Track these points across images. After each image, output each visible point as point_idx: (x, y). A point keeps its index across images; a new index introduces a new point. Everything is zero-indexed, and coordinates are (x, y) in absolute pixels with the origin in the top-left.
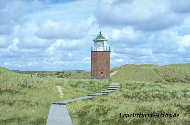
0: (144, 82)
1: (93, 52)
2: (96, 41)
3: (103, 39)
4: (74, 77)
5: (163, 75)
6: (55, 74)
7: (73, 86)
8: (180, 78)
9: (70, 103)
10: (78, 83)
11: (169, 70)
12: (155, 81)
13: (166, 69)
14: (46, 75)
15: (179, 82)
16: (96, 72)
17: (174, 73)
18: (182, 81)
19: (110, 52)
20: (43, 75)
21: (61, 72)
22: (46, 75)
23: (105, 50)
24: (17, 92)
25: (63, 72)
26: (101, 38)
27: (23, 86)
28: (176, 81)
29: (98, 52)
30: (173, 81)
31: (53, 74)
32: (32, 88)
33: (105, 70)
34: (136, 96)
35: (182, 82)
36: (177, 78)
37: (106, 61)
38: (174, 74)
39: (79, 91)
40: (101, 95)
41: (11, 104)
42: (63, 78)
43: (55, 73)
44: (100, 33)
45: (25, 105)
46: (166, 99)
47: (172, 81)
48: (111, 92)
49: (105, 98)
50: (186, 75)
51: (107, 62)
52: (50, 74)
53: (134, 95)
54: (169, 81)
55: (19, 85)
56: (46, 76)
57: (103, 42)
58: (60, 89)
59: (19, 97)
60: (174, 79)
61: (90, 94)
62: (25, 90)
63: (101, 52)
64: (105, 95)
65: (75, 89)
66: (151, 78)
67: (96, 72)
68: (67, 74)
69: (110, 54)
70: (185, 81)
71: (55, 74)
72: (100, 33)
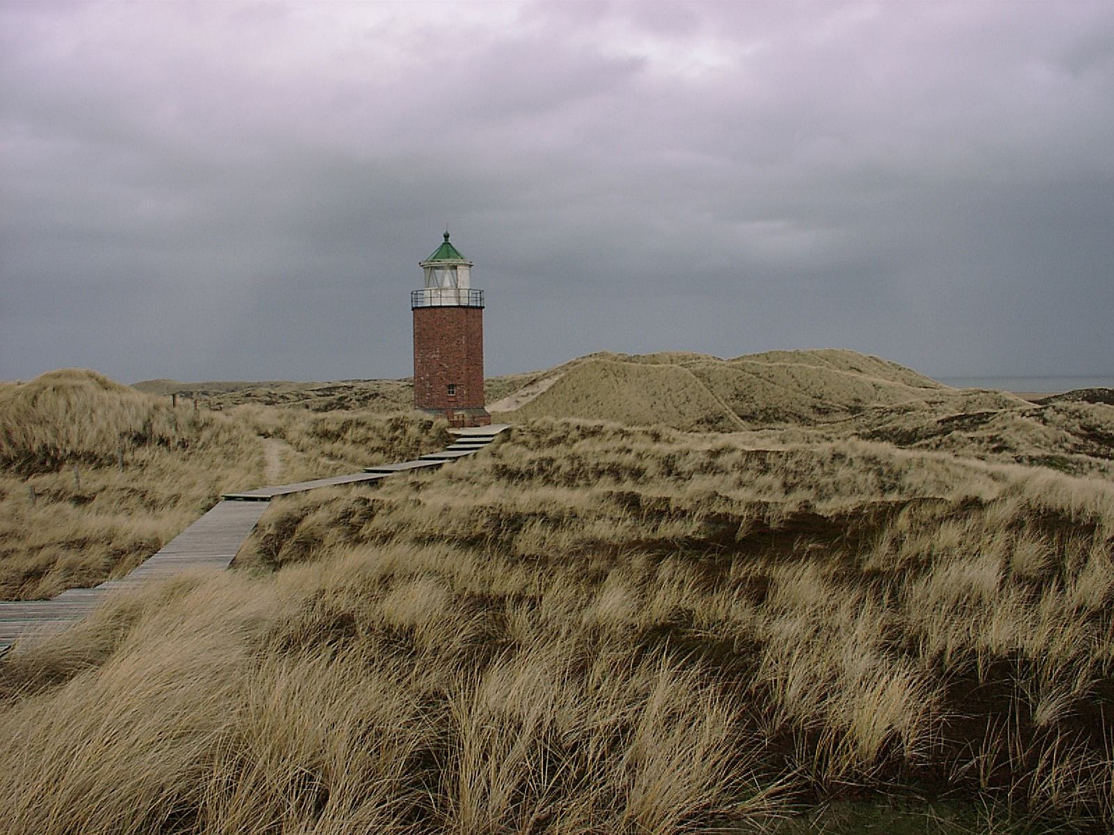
0: (599, 422)
1: (417, 308)
2: (430, 268)
3: (455, 262)
4: (389, 403)
5: (729, 392)
6: (319, 393)
7: (326, 435)
8: (797, 407)
9: (287, 494)
10: (346, 426)
11: (754, 377)
12: (696, 419)
13: (743, 373)
14: (282, 397)
15: (787, 422)
16: (428, 385)
17: (772, 385)
18: (800, 417)
19: (481, 308)
20: (269, 399)
21: (344, 384)
22: (282, 397)
23: (464, 302)
24: (113, 461)
25: (350, 384)
26: (448, 258)
27: (141, 439)
28: (777, 419)
29: (438, 311)
30: (767, 419)
31: (311, 393)
32: (172, 444)
33: (463, 378)
34: (541, 470)
35: (802, 420)
36: (780, 405)
37: (467, 342)
38: (771, 392)
39: (342, 457)
40: (412, 470)
41: (81, 500)
42: (347, 408)
43: (317, 390)
44: (446, 236)
45: (134, 500)
46: (641, 479)
47: (761, 417)
48: (456, 458)
49: (425, 477)
50: (819, 395)
51: (471, 346)
52: (297, 396)
53: (535, 467)
54: (752, 418)
55: (122, 435)
56: (281, 401)
57: (454, 271)
58: (274, 449)
59: (115, 477)
60: (770, 412)
61: (377, 465)
62: (143, 454)
63: (424, 311)
64: (431, 467)
65: (328, 447)
66: (682, 408)
67: (428, 385)
68: (363, 393)
69: (481, 317)
70: (813, 417)
71: (319, 393)
72: (446, 236)
